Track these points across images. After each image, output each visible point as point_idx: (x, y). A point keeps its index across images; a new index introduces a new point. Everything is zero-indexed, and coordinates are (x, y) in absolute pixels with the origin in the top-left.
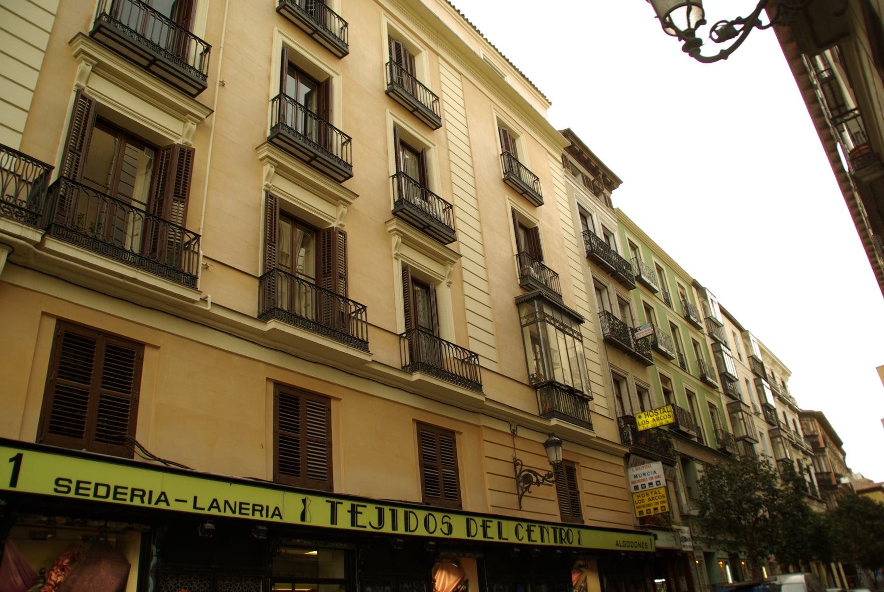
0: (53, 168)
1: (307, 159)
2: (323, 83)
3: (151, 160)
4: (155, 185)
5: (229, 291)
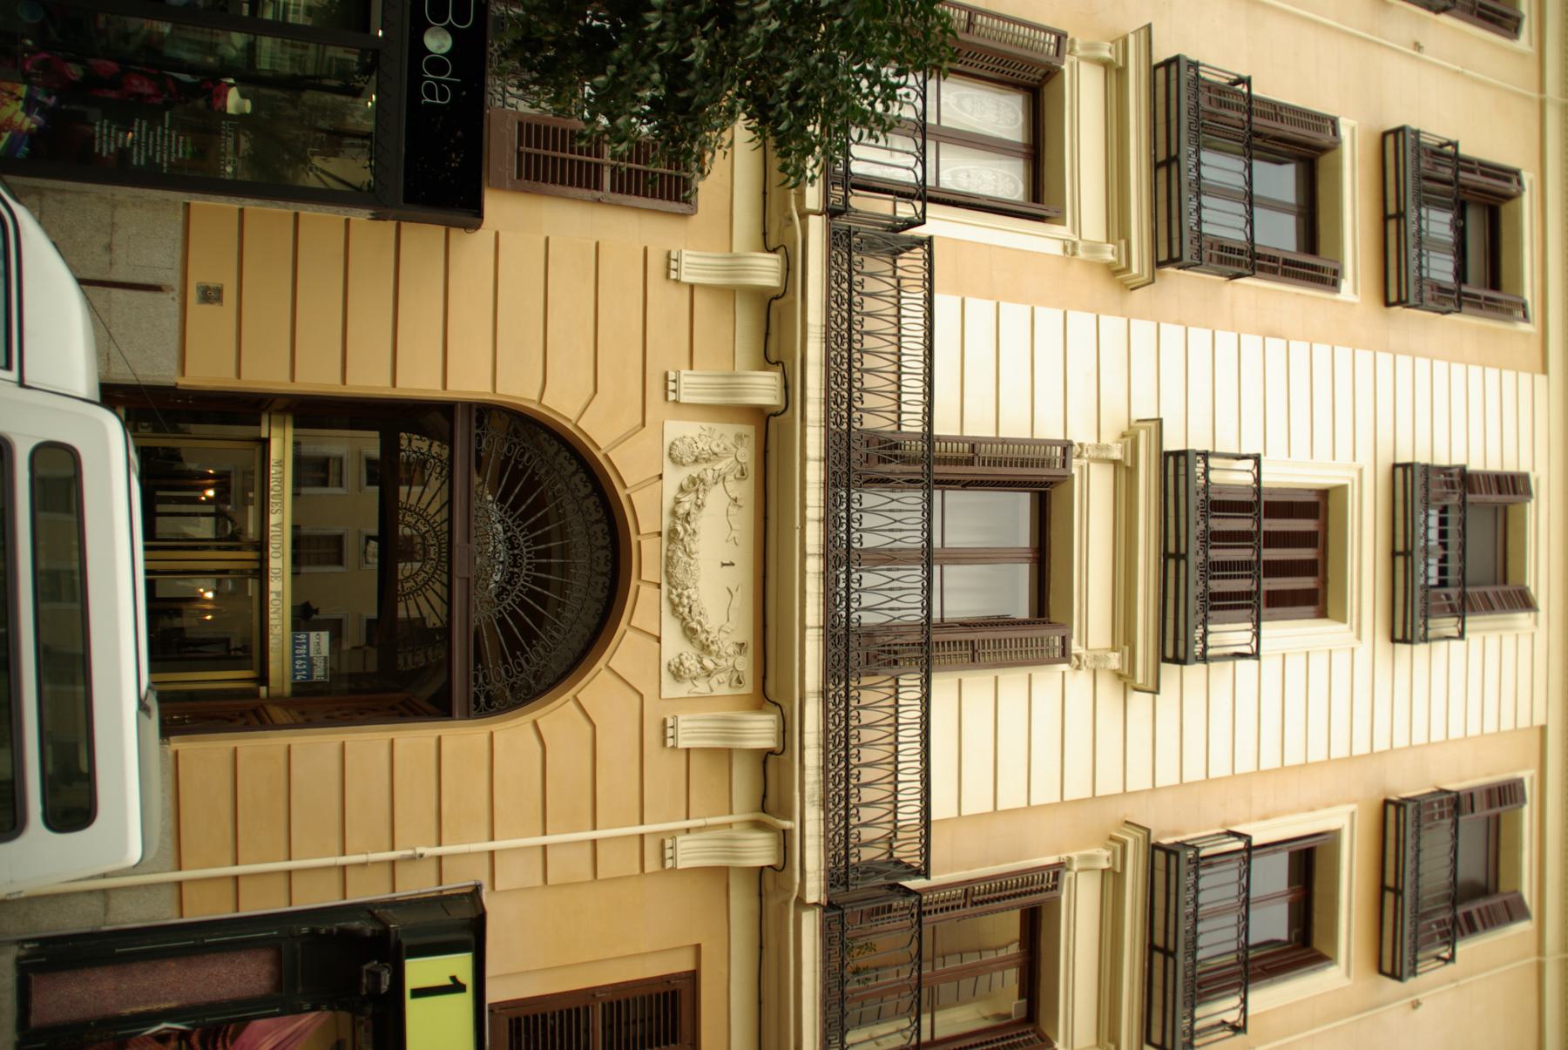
0: (927, 875)
2: (1314, 951)
3: (1009, 1016)
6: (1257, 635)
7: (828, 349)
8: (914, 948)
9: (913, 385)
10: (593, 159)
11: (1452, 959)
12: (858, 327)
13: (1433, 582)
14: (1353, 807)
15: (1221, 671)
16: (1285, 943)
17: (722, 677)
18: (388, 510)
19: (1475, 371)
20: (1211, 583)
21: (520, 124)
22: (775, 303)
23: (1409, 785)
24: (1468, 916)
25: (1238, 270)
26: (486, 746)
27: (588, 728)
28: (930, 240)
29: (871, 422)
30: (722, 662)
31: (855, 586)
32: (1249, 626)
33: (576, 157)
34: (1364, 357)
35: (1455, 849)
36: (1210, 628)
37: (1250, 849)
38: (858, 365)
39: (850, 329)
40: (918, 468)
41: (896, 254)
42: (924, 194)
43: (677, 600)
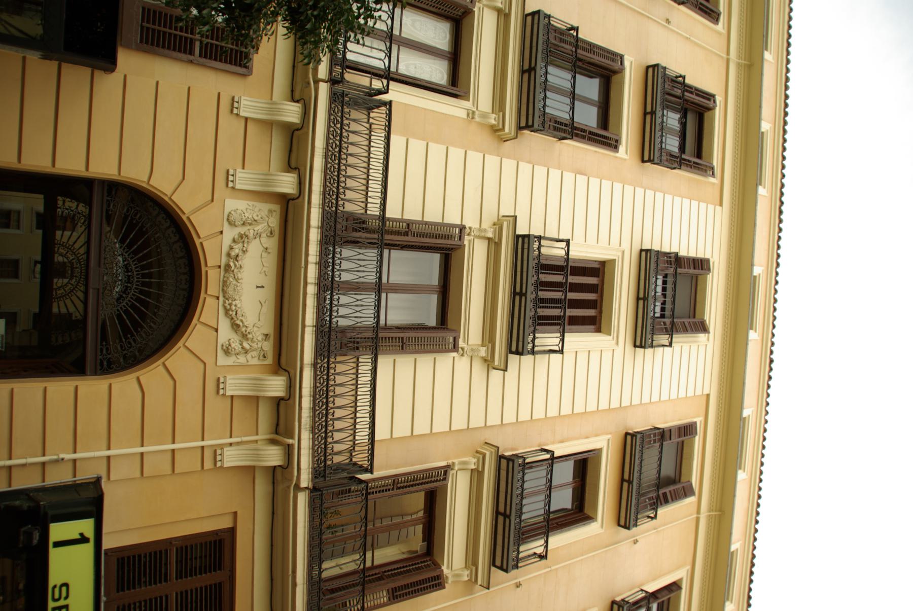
0: (371, 472)
1: (501, 509)
4: (395, 566)
6: (563, 340)
7: (326, 162)
8: (363, 513)
9: (375, 187)
10: (189, 36)
11: (655, 517)
12: (345, 151)
13: (658, 315)
14: (609, 436)
15: (541, 359)
16: (569, 510)
17: (254, 354)
18: (48, 246)
19: (686, 201)
20: (538, 310)
21: (144, 9)
22: (296, 133)
23: (639, 425)
24: (665, 494)
25: (564, 135)
26: (107, 392)
27: (171, 383)
28: (390, 103)
29: (349, 207)
30: (254, 345)
31: (336, 303)
32: (559, 335)
33: (178, 33)
34: (629, 189)
35: (660, 459)
36: (537, 335)
37: (553, 458)
38: (343, 173)
39: (340, 151)
40: (376, 236)
41: (370, 109)
42: (388, 75)
43: (228, 307)
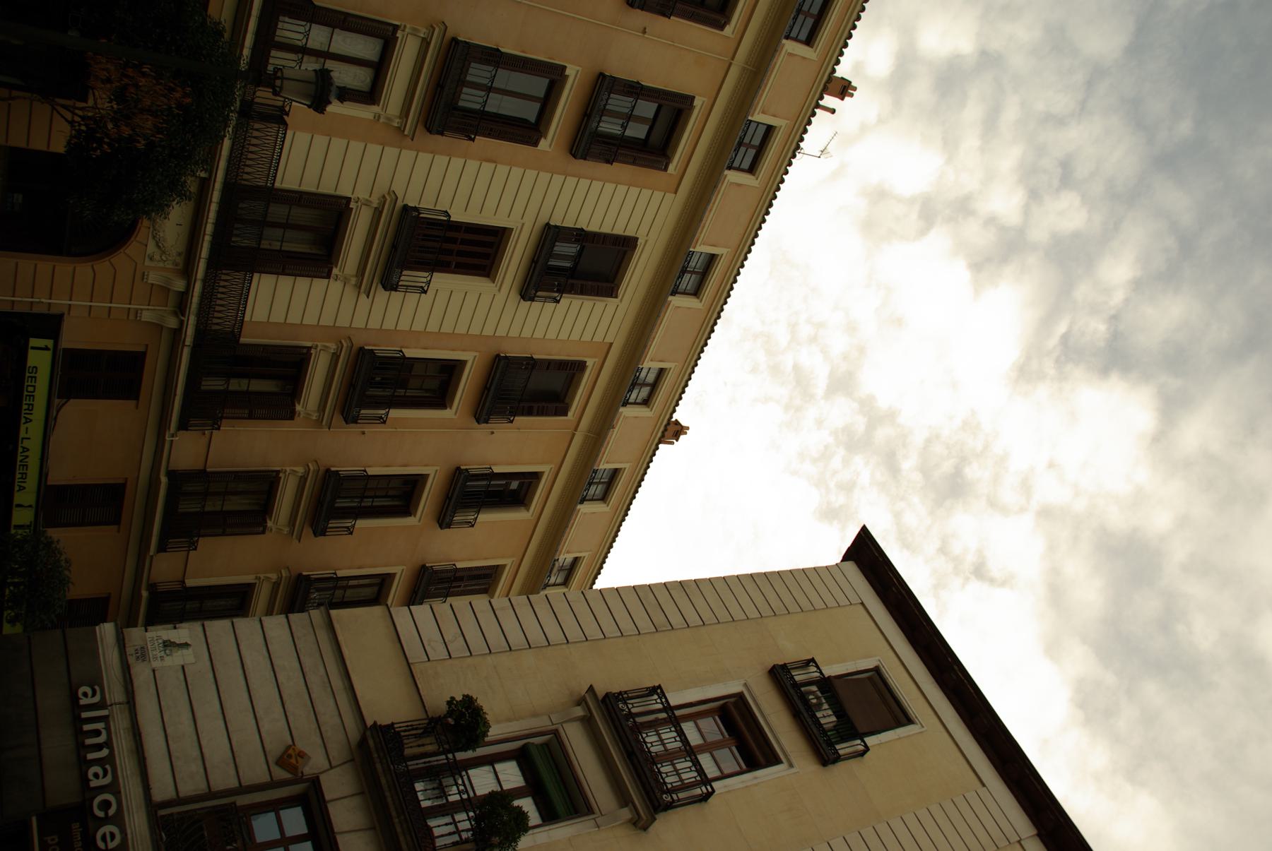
5: (187, 450)
23: (514, 351)
